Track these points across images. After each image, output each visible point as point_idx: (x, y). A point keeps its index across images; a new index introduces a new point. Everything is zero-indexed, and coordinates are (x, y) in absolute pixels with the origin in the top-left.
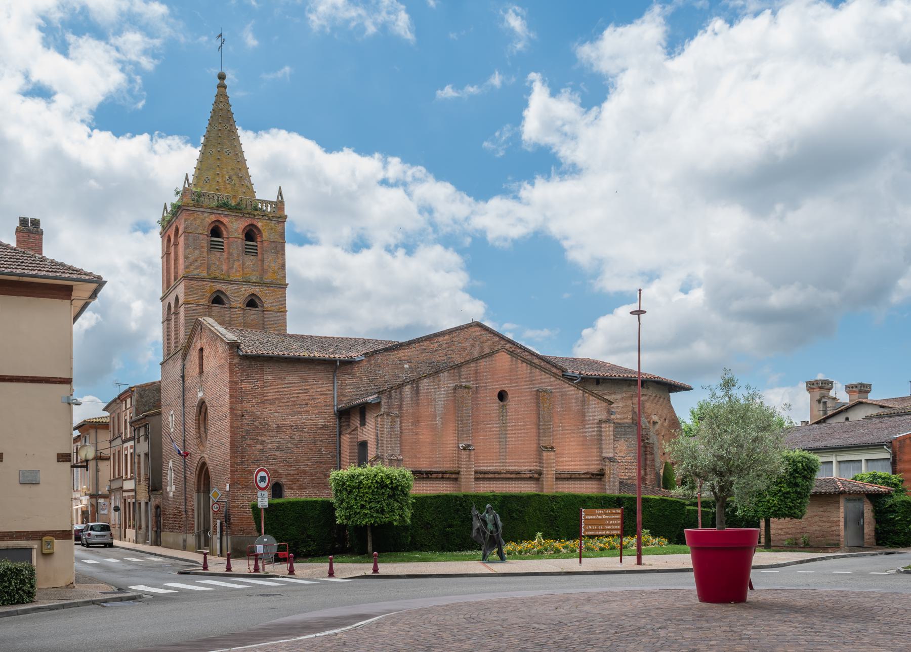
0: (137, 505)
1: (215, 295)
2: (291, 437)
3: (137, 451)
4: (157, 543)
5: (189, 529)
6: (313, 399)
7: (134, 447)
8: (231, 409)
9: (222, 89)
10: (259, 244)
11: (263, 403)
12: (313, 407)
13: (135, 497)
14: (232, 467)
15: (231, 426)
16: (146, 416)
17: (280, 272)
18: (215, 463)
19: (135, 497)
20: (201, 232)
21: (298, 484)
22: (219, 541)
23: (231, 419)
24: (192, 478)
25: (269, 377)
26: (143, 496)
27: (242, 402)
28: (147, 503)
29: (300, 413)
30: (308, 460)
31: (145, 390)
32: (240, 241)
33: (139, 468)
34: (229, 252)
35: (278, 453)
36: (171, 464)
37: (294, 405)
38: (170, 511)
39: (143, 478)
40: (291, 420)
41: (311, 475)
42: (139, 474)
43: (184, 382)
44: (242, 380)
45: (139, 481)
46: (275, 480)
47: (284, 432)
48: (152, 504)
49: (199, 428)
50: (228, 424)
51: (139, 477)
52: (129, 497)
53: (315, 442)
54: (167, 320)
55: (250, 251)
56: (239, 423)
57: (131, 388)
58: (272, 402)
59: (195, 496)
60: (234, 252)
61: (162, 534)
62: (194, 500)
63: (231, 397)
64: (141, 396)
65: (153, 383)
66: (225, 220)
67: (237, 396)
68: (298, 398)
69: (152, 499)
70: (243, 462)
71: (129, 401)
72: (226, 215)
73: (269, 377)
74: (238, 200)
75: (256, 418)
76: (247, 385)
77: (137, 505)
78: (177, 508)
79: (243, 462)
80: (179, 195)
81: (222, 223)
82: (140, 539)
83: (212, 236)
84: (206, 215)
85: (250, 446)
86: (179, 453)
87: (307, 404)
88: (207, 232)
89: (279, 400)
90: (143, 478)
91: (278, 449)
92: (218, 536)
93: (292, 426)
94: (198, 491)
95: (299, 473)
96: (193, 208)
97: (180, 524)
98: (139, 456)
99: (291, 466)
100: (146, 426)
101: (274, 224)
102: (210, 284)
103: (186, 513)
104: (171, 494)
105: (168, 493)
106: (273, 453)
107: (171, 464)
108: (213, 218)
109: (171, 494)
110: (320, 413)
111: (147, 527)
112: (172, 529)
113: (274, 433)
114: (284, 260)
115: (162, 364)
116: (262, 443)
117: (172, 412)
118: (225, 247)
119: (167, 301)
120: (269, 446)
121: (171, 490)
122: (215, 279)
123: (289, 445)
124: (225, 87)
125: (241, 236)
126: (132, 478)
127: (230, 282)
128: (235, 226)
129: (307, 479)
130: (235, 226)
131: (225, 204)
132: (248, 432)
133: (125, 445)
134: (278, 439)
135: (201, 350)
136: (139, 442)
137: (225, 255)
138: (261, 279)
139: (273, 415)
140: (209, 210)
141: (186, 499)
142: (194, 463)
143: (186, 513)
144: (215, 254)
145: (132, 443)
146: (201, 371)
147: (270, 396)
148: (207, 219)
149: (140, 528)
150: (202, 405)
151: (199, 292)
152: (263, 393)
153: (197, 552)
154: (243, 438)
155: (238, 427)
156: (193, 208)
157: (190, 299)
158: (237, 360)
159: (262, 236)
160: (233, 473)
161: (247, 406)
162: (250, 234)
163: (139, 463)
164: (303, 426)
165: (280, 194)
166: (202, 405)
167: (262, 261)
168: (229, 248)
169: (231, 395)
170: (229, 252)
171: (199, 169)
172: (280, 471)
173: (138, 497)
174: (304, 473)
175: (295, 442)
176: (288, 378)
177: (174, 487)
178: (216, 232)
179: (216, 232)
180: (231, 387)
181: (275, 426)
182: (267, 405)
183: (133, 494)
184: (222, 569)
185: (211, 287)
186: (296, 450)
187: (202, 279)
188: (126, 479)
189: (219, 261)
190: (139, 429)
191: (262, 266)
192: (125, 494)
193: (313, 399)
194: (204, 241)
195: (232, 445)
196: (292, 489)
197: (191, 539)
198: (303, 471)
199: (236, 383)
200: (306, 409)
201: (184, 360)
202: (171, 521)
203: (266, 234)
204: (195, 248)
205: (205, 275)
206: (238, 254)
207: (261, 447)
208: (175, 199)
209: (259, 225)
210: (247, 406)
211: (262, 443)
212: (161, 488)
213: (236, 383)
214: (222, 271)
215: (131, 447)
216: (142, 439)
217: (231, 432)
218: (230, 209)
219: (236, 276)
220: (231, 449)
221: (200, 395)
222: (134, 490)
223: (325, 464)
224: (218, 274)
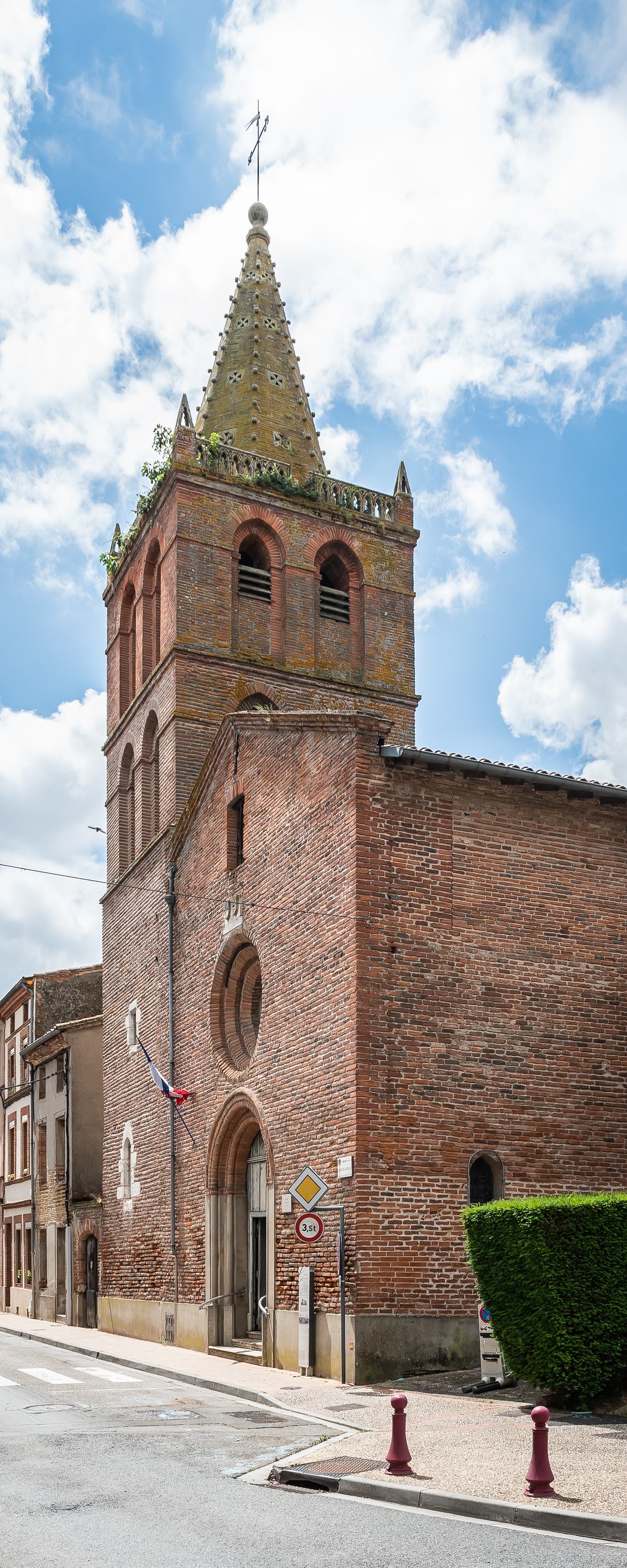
0: (38, 1236)
1: (327, 554)
2: (521, 1024)
3: (39, 1116)
4: (86, 1318)
5: (188, 1289)
6: (582, 917)
7: (31, 1110)
8: (361, 924)
9: (259, 241)
10: (352, 595)
11: (446, 915)
12: (582, 941)
13: (32, 1217)
14: (360, 1103)
15: (361, 980)
16: (63, 1030)
17: (402, 667)
18: (286, 1103)
19: (32, 1217)
20: (218, 543)
21: (539, 1163)
22: (304, 1330)
23: (361, 955)
24: (198, 1160)
25: (468, 842)
26: (51, 1217)
27: (390, 908)
28: (61, 1231)
29: (547, 956)
30: (567, 1093)
31: (56, 986)
32: (309, 578)
33: (43, 1153)
34: (284, 605)
35: (488, 1070)
36: (128, 1131)
37: (532, 928)
38: (124, 1242)
39: (51, 1176)
40: (526, 973)
41: (574, 1138)
42: (43, 1166)
43: (173, 913)
44: (391, 842)
45: (43, 1181)
46: (479, 1148)
47: (505, 1008)
48: (78, 1228)
49: (222, 1022)
50: (351, 974)
51: (43, 1174)
52: (18, 1219)
53: (584, 1043)
54: (121, 793)
55: (333, 608)
56: (384, 971)
57: (25, 980)
58: (474, 916)
59: (207, 1205)
60: (296, 603)
61: (102, 1301)
62: (205, 1214)
63: (361, 888)
64: (48, 997)
65: (74, 971)
66: (276, 522)
67: (378, 891)
68: (542, 910)
69: (76, 1222)
70: (391, 1091)
71: (19, 1014)
72: (278, 511)
73: (468, 842)
74: (308, 478)
75: (429, 961)
76: (408, 860)
77: (38, 1236)
78: (145, 1239)
79: (391, 1091)
80: (169, 447)
81: (267, 528)
82: (45, 1308)
83: (241, 562)
84: (230, 502)
85: (411, 1043)
86: (166, 1090)
87: (565, 930)
88: (232, 545)
89: (491, 910)
90: (51, 1176)
91: (488, 1057)
92: (304, 1311)
93: (525, 991)
94: (217, 1189)
95: (544, 1130)
96: (200, 481)
97: (156, 1273)
98: (43, 1127)
99: (522, 1110)
100: (61, 1057)
101: (388, 548)
102: (237, 675)
103: (177, 1247)
104: (128, 1206)
105: (118, 1203)
106: (474, 1067)
107: (128, 1131)
108: (248, 512)
109: (128, 1206)
110: (599, 959)
111: (61, 1283)
112: (130, 1290)
113: (480, 1010)
114: (410, 638)
115: (104, 901)
116: (446, 1036)
117: (133, 1005)
118: (275, 592)
119: (120, 747)
120: (465, 1047)
121: (127, 1192)
122: (251, 665)
123: (519, 1049)
124: (265, 238)
125: (312, 567)
126: (25, 1178)
127: (285, 677)
128: (299, 542)
129: (562, 1151)
130: (299, 542)
131: (274, 480)
132: (405, 998)
133: (9, 1111)
134: (488, 1028)
135: (238, 805)
136: (42, 1095)
137: (274, 612)
138: (359, 679)
139: (478, 955)
140: (237, 491)
141: (176, 1214)
142: (210, 1114)
143: (177, 1247)
144: (251, 606)
145: (26, 1101)
146: (237, 857)
147: (470, 898)
148: (233, 514)
149: (43, 1285)
150: (241, 951)
151: (212, 694)
152: (449, 889)
153: (211, 1352)
154: (394, 1019)
155: (378, 985)
156: (200, 481)
157: (191, 706)
158: (377, 779)
159: (360, 575)
160: (364, 1124)
161: (406, 921)
162: (335, 567)
163: (43, 1143)
164: (555, 991)
165: (404, 483)
166: (241, 951)
167: (361, 636)
168: (283, 598)
169: (359, 884)
170: (284, 605)
171: (218, 384)
172: (493, 1122)
173: (40, 1218)
174: (554, 1131)
175: (534, 1040)
176: (516, 848)
177: (136, 1189)
178: (251, 552)
179: (251, 552)
180: (362, 860)
181: (480, 989)
182: (459, 923)
183: (28, 1210)
184: (508, 1483)
185: (241, 684)
186: (534, 1063)
187: (220, 661)
188: (12, 1182)
189: (258, 625)
190: (42, 1066)
191: (362, 650)
192: (9, 1214)
193: (582, 917)
194: (227, 569)
195: (363, 1036)
196: (523, 1177)
197: (194, 1317)
198: (555, 1126)
199: (376, 847)
200: (563, 944)
201: (175, 858)
202: (126, 1270)
203: (370, 571)
204: (203, 582)
205: (226, 653)
206: (305, 609)
207: (442, 1047)
208: (160, 459)
209: (356, 545)
210: (406, 921)
211: (446, 1036)
212: (100, 1192)
213: (376, 847)
214: (265, 649)
215: (24, 1111)
216: (51, 1084)
217: (360, 997)
218: (290, 494)
219: (298, 661)
220: (361, 1048)
221: (231, 926)
222: (31, 1203)
223: (609, 1108)
224: (257, 654)
